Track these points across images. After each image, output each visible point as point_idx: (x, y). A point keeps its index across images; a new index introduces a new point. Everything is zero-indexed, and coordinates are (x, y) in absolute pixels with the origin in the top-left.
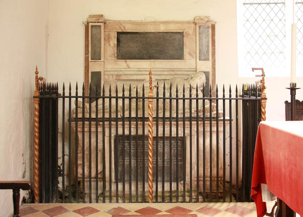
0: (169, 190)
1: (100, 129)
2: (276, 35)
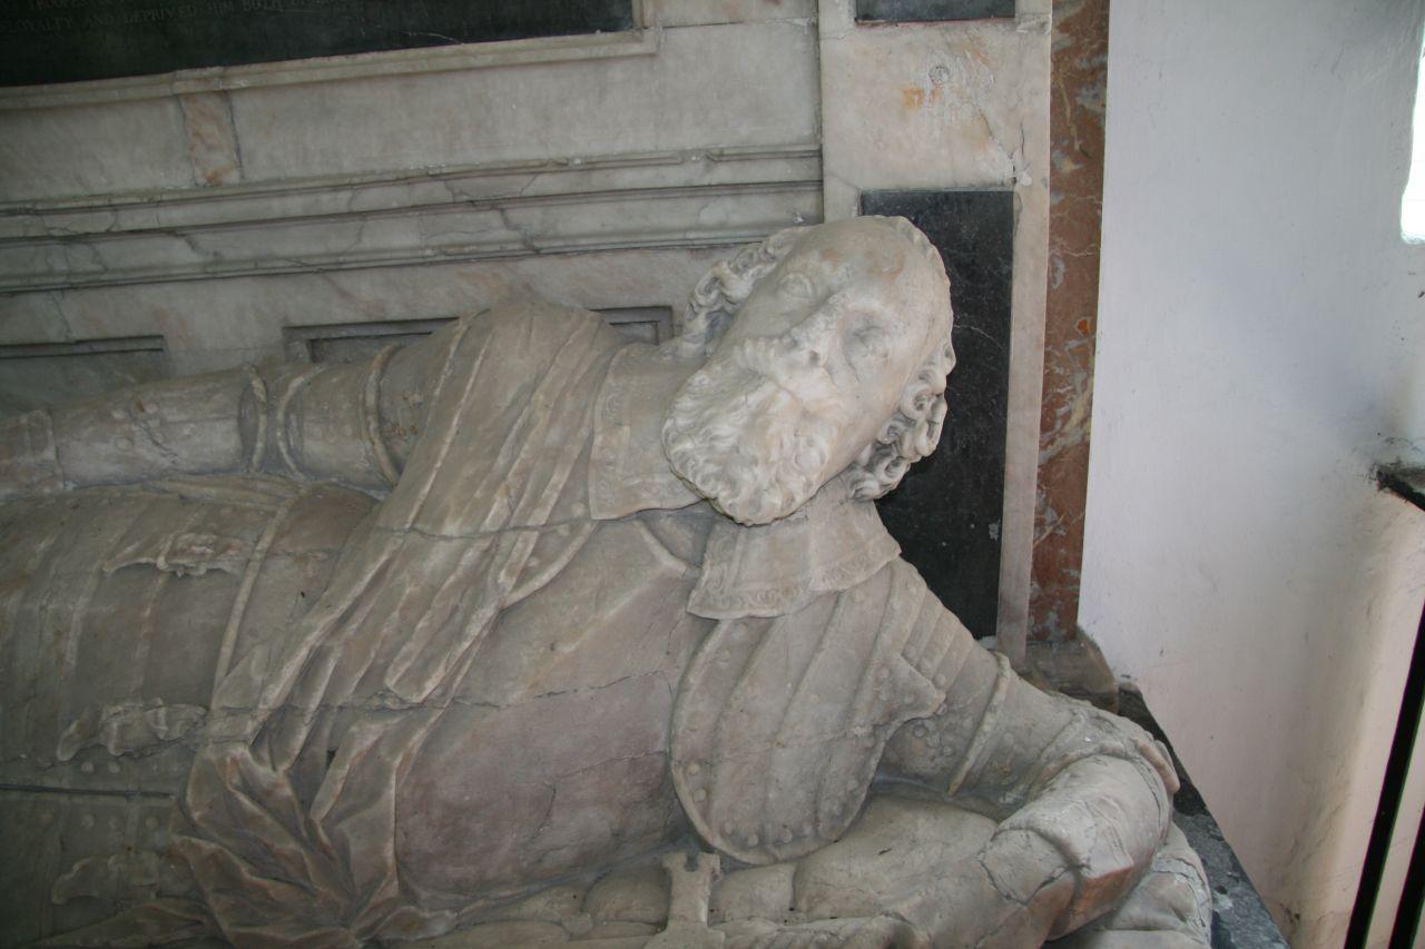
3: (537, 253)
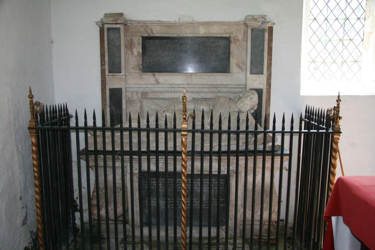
0: (208, 236)
1: (118, 164)
2: (350, 39)
3: (219, 92)
